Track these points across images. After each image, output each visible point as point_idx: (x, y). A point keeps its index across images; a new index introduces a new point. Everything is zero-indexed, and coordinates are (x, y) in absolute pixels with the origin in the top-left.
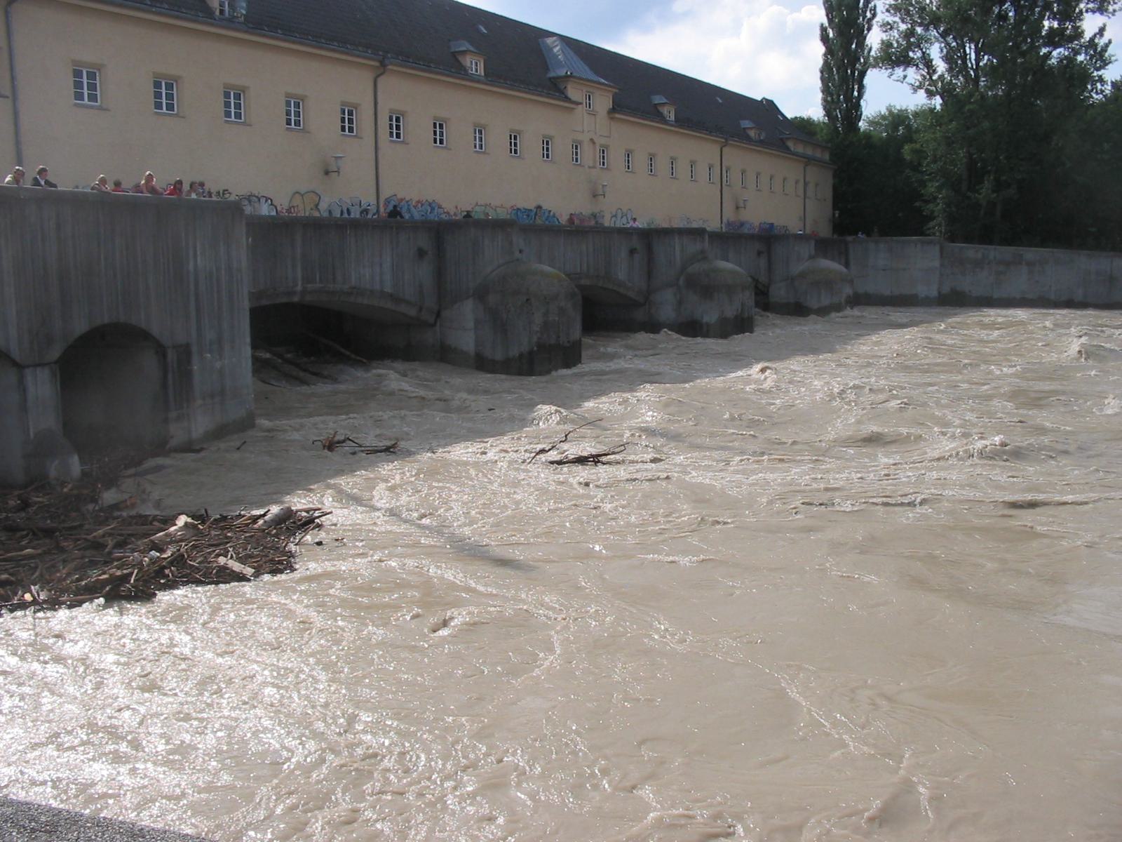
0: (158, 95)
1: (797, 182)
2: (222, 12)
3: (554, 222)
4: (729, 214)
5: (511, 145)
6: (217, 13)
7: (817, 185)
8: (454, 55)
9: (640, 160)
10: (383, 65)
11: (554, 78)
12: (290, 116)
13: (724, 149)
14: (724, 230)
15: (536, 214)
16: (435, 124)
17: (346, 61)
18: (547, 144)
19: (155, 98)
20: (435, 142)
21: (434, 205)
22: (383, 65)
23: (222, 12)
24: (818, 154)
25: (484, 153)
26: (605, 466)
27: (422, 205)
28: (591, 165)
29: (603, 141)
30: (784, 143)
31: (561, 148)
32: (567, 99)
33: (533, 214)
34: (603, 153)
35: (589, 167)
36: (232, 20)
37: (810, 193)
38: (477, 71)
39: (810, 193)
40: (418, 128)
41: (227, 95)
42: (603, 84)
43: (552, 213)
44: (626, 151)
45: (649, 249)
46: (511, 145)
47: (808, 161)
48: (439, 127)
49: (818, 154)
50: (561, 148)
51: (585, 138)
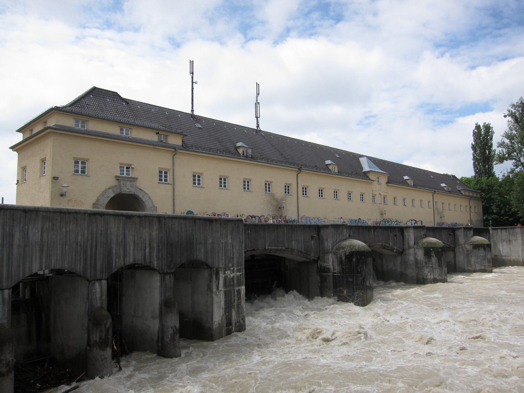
0: (221, 182)
1: (466, 206)
2: (243, 154)
3: (366, 224)
4: (438, 220)
5: (335, 195)
6: (242, 155)
7: (475, 207)
8: (327, 165)
9: (399, 201)
10: (300, 170)
11: (365, 172)
12: (245, 186)
13: (434, 195)
14: (275, 223)
15: (358, 221)
16: (348, 193)
17: (249, 163)
18: (385, 198)
19: (193, 181)
20: (348, 199)
21: (319, 219)
22: (300, 170)
23: (243, 154)
24: (475, 195)
25: (386, 204)
26: (332, 342)
27: (315, 219)
28: (380, 203)
29: (384, 194)
30: (460, 192)
31: (368, 197)
32: (370, 179)
33: (357, 221)
34: (385, 198)
35: (379, 204)
36: (247, 157)
37: (472, 210)
38: (335, 170)
39: (472, 210)
40: (313, 192)
41: (244, 182)
42: (385, 173)
43: (365, 221)
44: (403, 198)
45: (454, 233)
46: (335, 195)
47: (471, 198)
48: (336, 193)
49: (475, 195)
50: (368, 197)
51: (377, 193)
